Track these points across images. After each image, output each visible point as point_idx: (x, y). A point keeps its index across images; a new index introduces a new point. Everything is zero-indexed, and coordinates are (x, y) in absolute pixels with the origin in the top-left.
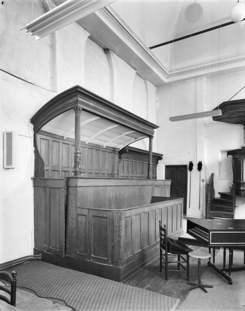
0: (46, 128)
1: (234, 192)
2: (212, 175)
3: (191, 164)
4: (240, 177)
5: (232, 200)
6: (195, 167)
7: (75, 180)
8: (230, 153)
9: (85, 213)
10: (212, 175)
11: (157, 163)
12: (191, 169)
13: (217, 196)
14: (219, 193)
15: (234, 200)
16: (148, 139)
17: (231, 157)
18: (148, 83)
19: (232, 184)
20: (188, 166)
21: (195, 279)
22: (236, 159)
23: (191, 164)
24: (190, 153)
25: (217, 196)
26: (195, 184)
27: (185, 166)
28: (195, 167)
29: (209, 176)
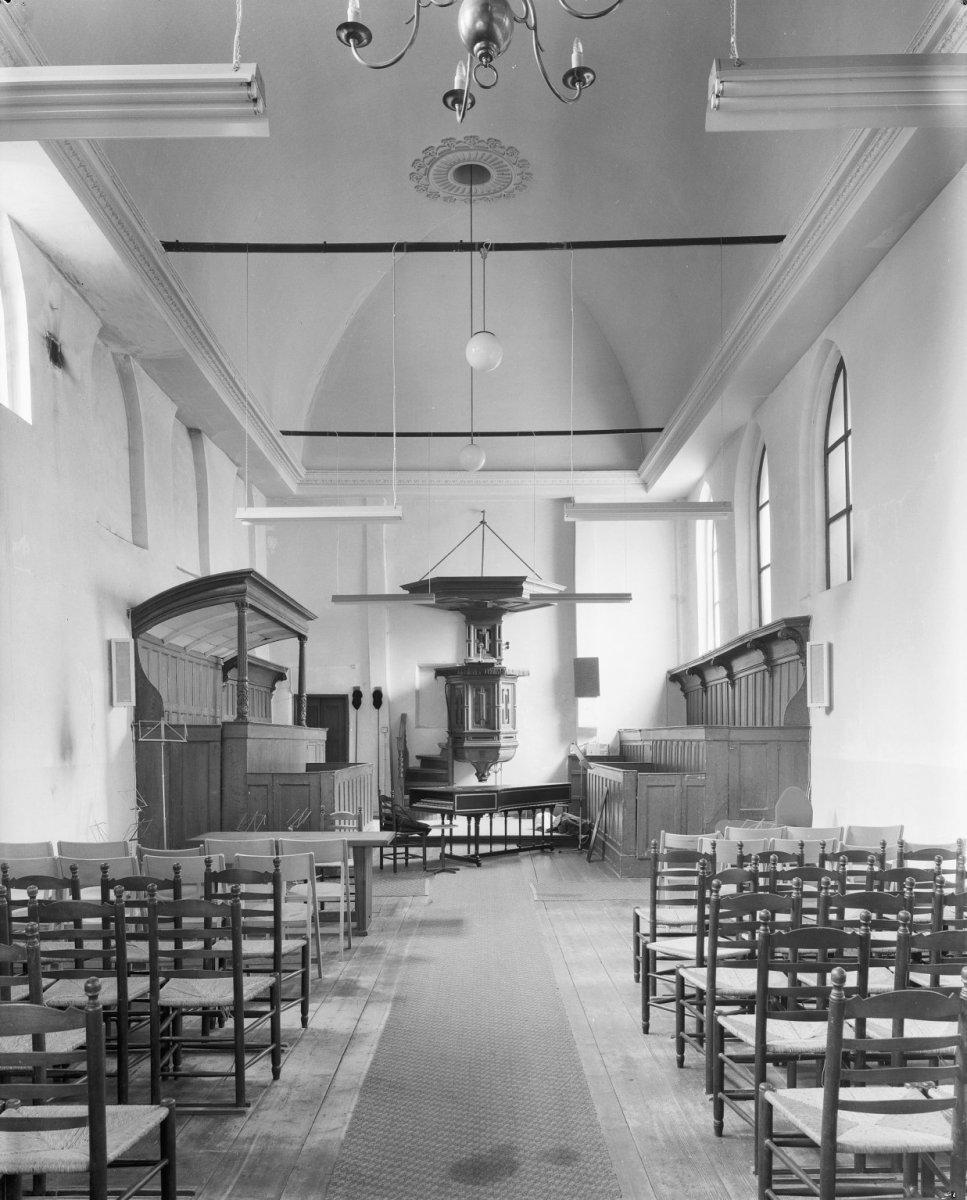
0: (158, 631)
1: (450, 751)
2: (404, 717)
3: (358, 694)
4: (463, 723)
5: (447, 769)
6: (367, 699)
7: (242, 727)
8: (441, 672)
9: (266, 782)
10: (404, 717)
11: (273, 689)
12: (357, 704)
13: (414, 763)
14: (418, 757)
15: (450, 769)
16: (296, 641)
17: (442, 680)
18: (256, 492)
19: (442, 741)
20: (351, 699)
21: (451, 856)
22: (454, 685)
23: (357, 694)
24: (353, 667)
25: (414, 763)
26: (367, 736)
27: (344, 698)
28: (367, 699)
29: (397, 718)
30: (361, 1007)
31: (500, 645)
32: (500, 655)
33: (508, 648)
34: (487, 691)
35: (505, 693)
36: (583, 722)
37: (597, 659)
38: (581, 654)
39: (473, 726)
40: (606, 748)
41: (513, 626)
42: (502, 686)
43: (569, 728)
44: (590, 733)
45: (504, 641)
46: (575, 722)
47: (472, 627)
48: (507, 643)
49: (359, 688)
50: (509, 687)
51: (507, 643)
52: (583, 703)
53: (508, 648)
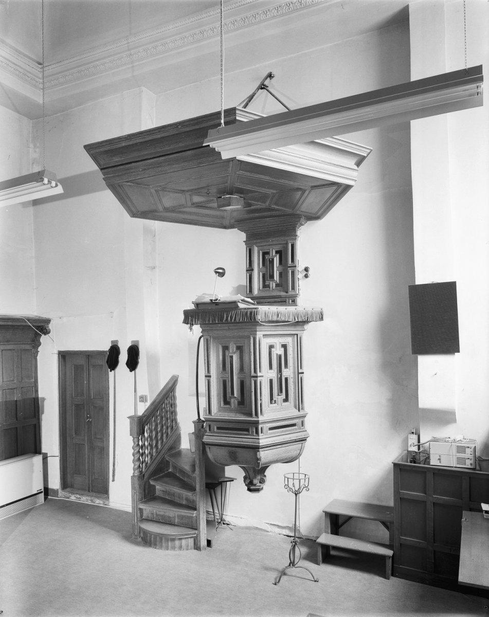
6: (123, 357)
28: (123, 357)
30: (302, 552)
31: (293, 273)
32: (293, 288)
33: (306, 276)
34: (240, 348)
35: (278, 351)
36: (427, 399)
37: (409, 286)
38: (423, 277)
39: (220, 409)
40: (468, 454)
41: (310, 242)
42: (265, 343)
43: (403, 405)
44: (444, 417)
45: (300, 267)
46: (414, 396)
47: (256, 249)
48: (306, 269)
49: (117, 341)
50: (289, 341)
51: (306, 269)
52: (428, 364)
53: (306, 276)
